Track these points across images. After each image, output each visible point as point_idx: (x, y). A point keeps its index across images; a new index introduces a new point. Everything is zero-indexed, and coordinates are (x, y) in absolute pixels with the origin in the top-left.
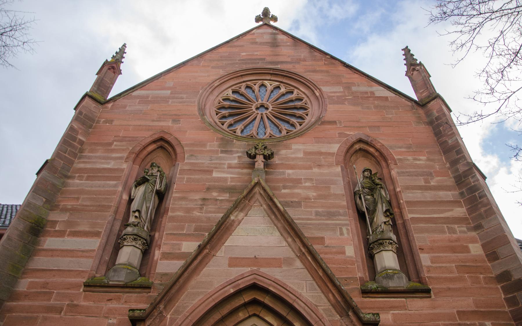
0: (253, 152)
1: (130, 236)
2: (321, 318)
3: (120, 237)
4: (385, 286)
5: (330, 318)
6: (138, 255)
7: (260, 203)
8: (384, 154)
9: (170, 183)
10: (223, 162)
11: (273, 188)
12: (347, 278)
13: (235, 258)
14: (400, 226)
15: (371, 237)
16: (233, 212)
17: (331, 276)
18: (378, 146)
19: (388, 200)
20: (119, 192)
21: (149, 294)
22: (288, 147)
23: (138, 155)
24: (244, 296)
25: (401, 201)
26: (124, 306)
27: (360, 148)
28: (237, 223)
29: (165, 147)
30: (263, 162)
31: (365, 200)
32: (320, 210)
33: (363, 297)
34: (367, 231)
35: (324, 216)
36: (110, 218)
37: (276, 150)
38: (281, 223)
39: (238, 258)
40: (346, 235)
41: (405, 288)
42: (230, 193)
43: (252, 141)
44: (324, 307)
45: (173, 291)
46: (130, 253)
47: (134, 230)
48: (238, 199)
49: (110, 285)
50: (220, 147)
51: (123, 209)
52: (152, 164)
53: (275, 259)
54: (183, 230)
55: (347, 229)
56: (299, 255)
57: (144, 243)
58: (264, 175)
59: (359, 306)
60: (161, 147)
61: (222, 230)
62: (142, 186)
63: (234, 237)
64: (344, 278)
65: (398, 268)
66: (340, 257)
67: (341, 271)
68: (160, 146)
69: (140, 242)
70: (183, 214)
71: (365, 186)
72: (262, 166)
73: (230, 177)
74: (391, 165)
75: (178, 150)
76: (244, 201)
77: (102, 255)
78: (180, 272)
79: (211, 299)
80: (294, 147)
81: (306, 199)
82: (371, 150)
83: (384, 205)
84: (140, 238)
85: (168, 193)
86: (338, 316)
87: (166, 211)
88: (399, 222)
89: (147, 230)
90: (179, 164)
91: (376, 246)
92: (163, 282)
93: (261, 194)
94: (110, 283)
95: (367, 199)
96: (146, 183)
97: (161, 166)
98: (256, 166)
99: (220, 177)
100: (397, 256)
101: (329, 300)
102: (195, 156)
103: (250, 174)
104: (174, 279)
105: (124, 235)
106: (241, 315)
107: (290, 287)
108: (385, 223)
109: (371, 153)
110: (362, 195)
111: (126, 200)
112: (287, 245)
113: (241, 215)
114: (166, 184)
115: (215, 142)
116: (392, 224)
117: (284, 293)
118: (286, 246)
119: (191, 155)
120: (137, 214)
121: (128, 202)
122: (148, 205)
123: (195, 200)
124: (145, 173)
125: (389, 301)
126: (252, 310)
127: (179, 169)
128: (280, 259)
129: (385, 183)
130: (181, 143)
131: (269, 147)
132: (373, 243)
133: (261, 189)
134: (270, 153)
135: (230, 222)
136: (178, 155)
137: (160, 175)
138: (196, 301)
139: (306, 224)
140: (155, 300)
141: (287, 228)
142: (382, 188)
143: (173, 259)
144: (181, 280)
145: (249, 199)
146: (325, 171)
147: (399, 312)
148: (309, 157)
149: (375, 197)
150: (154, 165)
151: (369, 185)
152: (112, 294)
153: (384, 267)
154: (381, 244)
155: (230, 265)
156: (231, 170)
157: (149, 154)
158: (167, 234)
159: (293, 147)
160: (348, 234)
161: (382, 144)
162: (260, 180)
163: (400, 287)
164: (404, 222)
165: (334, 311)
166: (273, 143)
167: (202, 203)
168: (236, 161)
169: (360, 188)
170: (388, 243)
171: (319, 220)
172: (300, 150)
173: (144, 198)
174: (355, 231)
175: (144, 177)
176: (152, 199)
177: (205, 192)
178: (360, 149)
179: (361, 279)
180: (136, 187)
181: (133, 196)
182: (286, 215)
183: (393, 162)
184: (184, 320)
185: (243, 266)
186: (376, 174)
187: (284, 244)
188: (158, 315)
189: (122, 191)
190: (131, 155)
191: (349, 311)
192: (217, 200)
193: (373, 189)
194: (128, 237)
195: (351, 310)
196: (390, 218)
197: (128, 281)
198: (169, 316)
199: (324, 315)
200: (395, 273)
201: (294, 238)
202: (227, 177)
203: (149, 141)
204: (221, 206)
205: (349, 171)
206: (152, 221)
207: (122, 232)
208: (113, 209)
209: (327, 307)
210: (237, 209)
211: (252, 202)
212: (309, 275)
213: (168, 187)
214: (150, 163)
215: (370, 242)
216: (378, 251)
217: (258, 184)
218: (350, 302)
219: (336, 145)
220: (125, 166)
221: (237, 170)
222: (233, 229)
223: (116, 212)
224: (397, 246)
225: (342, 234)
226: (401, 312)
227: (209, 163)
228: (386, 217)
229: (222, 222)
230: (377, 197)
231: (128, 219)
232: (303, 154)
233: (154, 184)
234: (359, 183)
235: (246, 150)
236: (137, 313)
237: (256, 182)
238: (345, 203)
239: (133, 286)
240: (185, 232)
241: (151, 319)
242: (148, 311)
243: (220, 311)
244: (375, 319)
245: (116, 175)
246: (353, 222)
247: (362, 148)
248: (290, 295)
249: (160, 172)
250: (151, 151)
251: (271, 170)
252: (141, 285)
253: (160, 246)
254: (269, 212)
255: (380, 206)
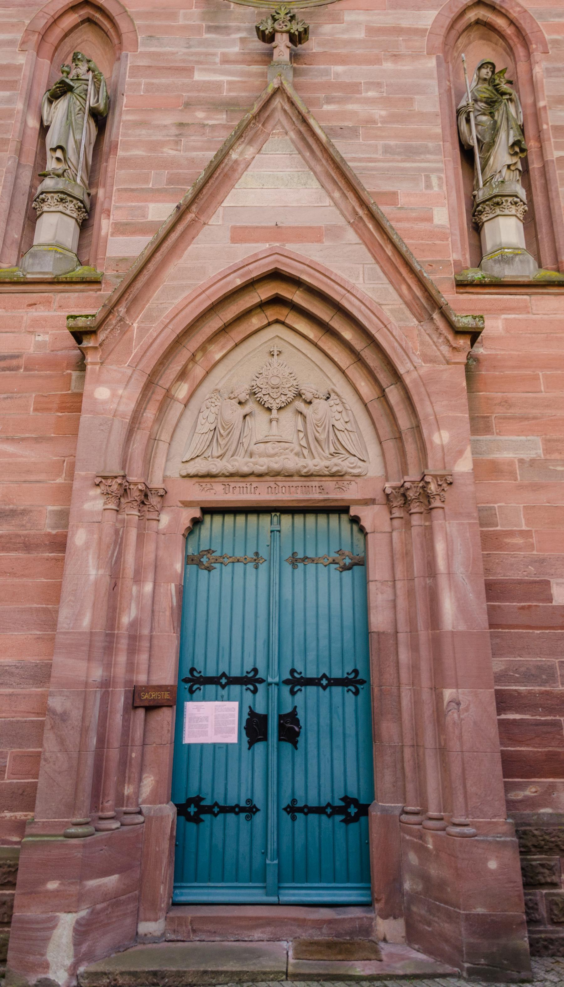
0: (268, 27)
1: (52, 195)
2: (386, 323)
3: (35, 198)
4: (496, 275)
5: (402, 324)
6: (72, 229)
7: (283, 128)
8: (524, 30)
9: (115, 96)
10: (212, 50)
11: (309, 102)
12: (433, 262)
13: (241, 228)
14: (536, 173)
15: (481, 193)
16: (236, 146)
17: (407, 255)
18: (514, 13)
19: (519, 123)
20: (18, 112)
21: (98, 293)
22: (336, 19)
23: (44, 37)
24: (259, 291)
25: (545, 127)
26: (59, 313)
27: (478, 19)
28: (242, 166)
29: (96, 21)
30: (288, 47)
31: (477, 125)
32: (392, 143)
33: (457, 293)
34: (475, 182)
35: (399, 154)
36: (10, 163)
37: (313, 25)
38: (322, 165)
39: (246, 227)
40: (436, 189)
41: (531, 279)
42: (229, 113)
43: (267, 6)
44: (393, 307)
45: (139, 284)
46: (57, 225)
47: (57, 184)
48: (242, 121)
49: (29, 280)
50: (203, 20)
51: (31, 145)
52: (76, 55)
53: (310, 227)
54: (147, 182)
55: (440, 178)
56: (352, 221)
57: (79, 207)
58: (291, 74)
59: (451, 305)
60: (89, 20)
61: (217, 178)
62: (62, 101)
63: (239, 190)
64: (426, 262)
65: (523, 246)
66: (423, 226)
67: (423, 251)
68: (85, 17)
69: (72, 205)
70: (144, 154)
71: (479, 97)
72: (286, 56)
73: (227, 81)
74: (535, 53)
75: (123, 25)
76: (254, 124)
77: (6, 231)
78: (147, 253)
79: (204, 296)
80: (349, 17)
81: (367, 122)
82: (500, 22)
83: (511, 132)
84: (71, 199)
85: (113, 114)
86: (415, 320)
87: (114, 147)
88: (535, 165)
89: (81, 184)
90: (127, 56)
91: (487, 208)
92: (121, 273)
93: (285, 111)
94: (29, 276)
95: (480, 122)
96: (69, 94)
97: (94, 60)
98: (275, 58)
99: (209, 82)
100: (524, 228)
101: (401, 296)
102: (158, 39)
103: (264, 75)
104: (138, 265)
105: (42, 193)
106: (256, 321)
107: (336, 275)
108: (509, 167)
109: (499, 29)
110: (472, 115)
111: (35, 129)
112: (332, 204)
113: (250, 151)
114: (108, 97)
115: (194, 9)
116: (521, 169)
117: (326, 284)
118: (330, 206)
119: (151, 36)
120: (59, 154)
121: (40, 133)
122: (78, 137)
123: (165, 126)
124: (63, 73)
125: (500, 300)
126: (272, 313)
127: (129, 65)
128: (320, 228)
129: (518, 91)
130: (126, 11)
131: (299, 17)
132: (484, 202)
133: (286, 100)
134: (301, 30)
135: (231, 163)
136: (124, 36)
137: (94, 77)
138: (179, 300)
139: (364, 169)
140: (110, 299)
141: (333, 174)
142: (511, 100)
143: (133, 233)
144: (151, 267)
145: (263, 120)
146: (406, 66)
147: (517, 316)
148: (376, 38)
149: (496, 118)
150: (79, 57)
151: (487, 95)
152: (34, 295)
153: (498, 243)
154: (498, 204)
155: (234, 240)
156: (227, 66)
157: (66, 35)
158: (118, 190)
159: (345, 19)
160: (440, 186)
161: (522, 7)
162: (284, 82)
163: (522, 276)
164: (544, 166)
165: (408, 313)
166: (307, 10)
167: (177, 132)
168: (236, 49)
169: (470, 100)
170: (511, 203)
171: (389, 161)
172: (360, 24)
173: (69, 124)
174: (452, 181)
175: (62, 82)
176: (85, 126)
177: (181, 111)
178: (478, 22)
179: (457, 263)
180: (50, 102)
181: (47, 121)
182: (331, 150)
183: (541, 48)
184: (162, 330)
185: (257, 241)
186: (502, 72)
187: (328, 201)
188: (117, 323)
189: (23, 111)
190: (30, 37)
191: (434, 311)
192: (204, 126)
193: (495, 102)
194: (49, 196)
195: (437, 311)
196: (520, 157)
197: (59, 273)
198: (135, 325)
199: (392, 319)
200: (517, 254)
201: (345, 192)
202: (221, 81)
203: (62, 6)
204: (213, 138)
205: (451, 67)
206: (89, 168)
207: (36, 189)
208: (12, 146)
209: (398, 307)
210: (243, 139)
211: (269, 126)
212: (369, 255)
213: (111, 103)
214: (72, 55)
215: (478, 201)
216: (491, 216)
217: (279, 90)
218: (436, 297)
219: (430, 12)
220: (21, 59)
221: (240, 67)
222: (237, 178)
223: (20, 152)
224: (526, 208)
225: (429, 186)
226: (520, 317)
227: (184, 54)
228: (512, 155)
229: (215, 163)
230: (500, 117)
231: (44, 167)
232: (366, 33)
233: (84, 97)
234: (469, 91)
235: (255, 24)
236: (81, 323)
237: (276, 86)
238: (439, 130)
239: (68, 280)
240: (150, 186)
241: (106, 330)
242: (99, 318)
243: (220, 315)
244: (476, 324)
245: (7, 79)
246: (451, 166)
247: (481, 18)
248: (336, 287)
249: (93, 71)
250: (70, 28)
251: (304, 66)
252: (83, 278)
253: (109, 212)
254: (300, 144)
255: (502, 135)
